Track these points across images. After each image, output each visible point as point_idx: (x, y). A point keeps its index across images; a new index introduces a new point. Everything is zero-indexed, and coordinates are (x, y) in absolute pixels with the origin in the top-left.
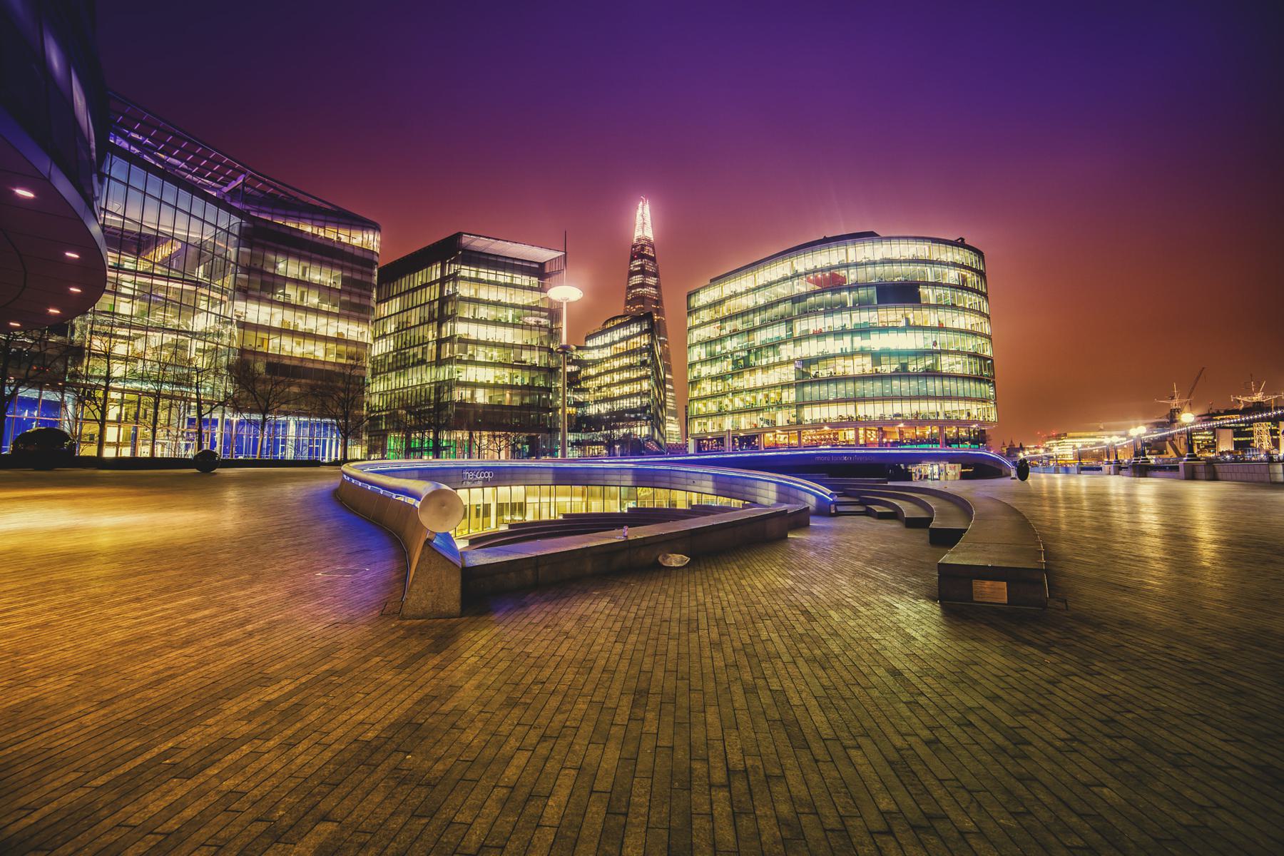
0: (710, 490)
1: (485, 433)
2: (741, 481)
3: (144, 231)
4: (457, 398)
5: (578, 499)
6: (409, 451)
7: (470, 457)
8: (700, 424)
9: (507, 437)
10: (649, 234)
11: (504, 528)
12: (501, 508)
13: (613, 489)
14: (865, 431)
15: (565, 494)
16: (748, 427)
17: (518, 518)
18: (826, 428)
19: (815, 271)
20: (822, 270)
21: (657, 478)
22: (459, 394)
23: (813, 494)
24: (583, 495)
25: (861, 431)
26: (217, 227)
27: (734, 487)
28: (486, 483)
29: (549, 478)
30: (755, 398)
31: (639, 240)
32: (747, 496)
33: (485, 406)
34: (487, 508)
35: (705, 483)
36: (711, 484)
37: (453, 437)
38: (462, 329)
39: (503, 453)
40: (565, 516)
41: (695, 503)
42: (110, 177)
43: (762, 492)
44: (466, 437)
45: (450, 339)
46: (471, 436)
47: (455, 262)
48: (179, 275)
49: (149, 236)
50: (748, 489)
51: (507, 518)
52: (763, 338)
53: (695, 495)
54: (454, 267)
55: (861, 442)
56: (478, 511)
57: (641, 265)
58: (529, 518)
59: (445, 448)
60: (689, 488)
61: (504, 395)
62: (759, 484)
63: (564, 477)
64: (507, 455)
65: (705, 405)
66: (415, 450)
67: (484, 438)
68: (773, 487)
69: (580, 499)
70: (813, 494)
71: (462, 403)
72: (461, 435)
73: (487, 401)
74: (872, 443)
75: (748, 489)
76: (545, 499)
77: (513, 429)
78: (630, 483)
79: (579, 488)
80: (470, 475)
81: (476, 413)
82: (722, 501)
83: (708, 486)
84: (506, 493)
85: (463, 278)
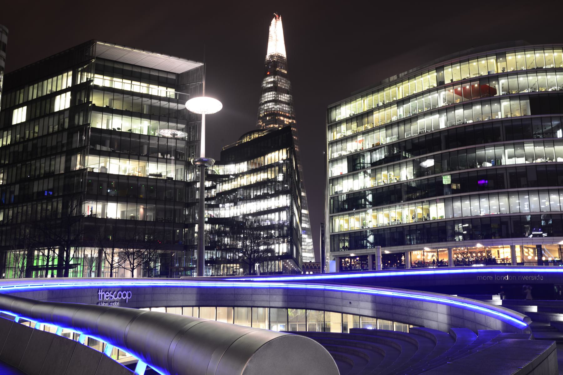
0: (369, 312)
1: (116, 250)
2: (339, 295)
4: (87, 213)
6: (29, 270)
7: (98, 274)
9: (140, 255)
10: (283, 52)
13: (261, 310)
14: (522, 248)
19: (463, 82)
20: (471, 80)
22: (77, 117)
25: (518, 248)
27: (396, 309)
30: (401, 214)
31: (272, 56)
32: (412, 320)
33: (116, 221)
35: (362, 304)
36: (369, 305)
37: (80, 255)
39: (135, 271)
43: (430, 315)
44: (96, 255)
46: (100, 253)
47: (88, 71)
50: (412, 311)
53: (350, 317)
54: (86, 76)
55: (519, 260)
57: (273, 82)
59: (71, 266)
60: (345, 309)
61: (137, 210)
62: (425, 305)
64: (139, 274)
65: (348, 222)
66: (37, 268)
67: (113, 255)
71: (92, 218)
72: (91, 252)
73: (119, 216)
74: (530, 262)
75: (412, 311)
77: (149, 245)
78: (280, 304)
81: (147, 187)
82: (381, 324)
83: (367, 308)
85: (96, 87)
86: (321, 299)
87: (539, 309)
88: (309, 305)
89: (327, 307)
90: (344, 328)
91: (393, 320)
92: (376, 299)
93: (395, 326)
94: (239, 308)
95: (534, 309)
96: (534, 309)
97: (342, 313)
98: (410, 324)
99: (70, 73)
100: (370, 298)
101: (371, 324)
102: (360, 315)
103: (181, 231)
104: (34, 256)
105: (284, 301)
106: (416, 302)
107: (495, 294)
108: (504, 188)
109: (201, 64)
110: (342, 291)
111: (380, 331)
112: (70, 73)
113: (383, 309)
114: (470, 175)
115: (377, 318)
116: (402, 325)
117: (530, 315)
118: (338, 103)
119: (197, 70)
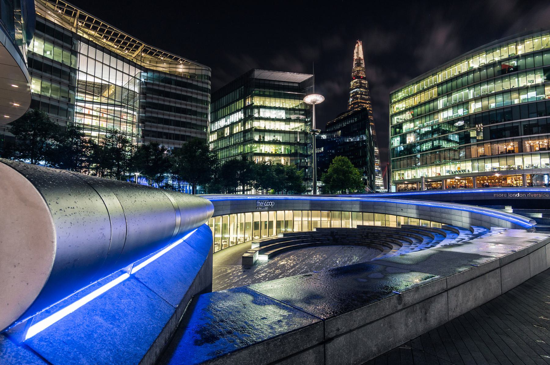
0: (415, 216)
2: (439, 210)
3: (104, 82)
5: (325, 219)
8: (399, 175)
11: (281, 236)
12: (279, 224)
15: (317, 216)
16: (434, 175)
17: (289, 230)
18: (497, 175)
21: (376, 207)
22: (258, 160)
23: (508, 220)
24: (328, 216)
26: (129, 75)
27: (433, 213)
28: (270, 209)
29: (357, 208)
32: (444, 220)
34: (271, 223)
35: (409, 210)
36: (415, 211)
38: (257, 124)
40: (317, 229)
41: (402, 223)
42: (80, 53)
43: (457, 218)
45: (250, 130)
48: (113, 102)
49: (106, 84)
50: (444, 215)
51: (283, 229)
52: (445, 116)
56: (266, 225)
58: (296, 230)
60: (398, 213)
62: (453, 212)
63: (315, 206)
64: (142, 116)
68: (467, 214)
69: (326, 219)
70: (508, 220)
75: (444, 215)
76: (305, 219)
79: (325, 213)
80: (261, 204)
83: (413, 212)
84: (281, 215)
86: (384, 207)
87: (543, 216)
88: (375, 211)
89: (387, 212)
90: (399, 224)
91: (431, 221)
92: (418, 207)
93: (432, 224)
94: (335, 212)
95: (540, 216)
96: (540, 216)
97: (397, 215)
98: (442, 223)
99: (243, 100)
100: (415, 207)
101: (414, 222)
102: (408, 217)
103: (372, 121)
104: (134, 172)
105: (360, 208)
106: (446, 210)
107: (507, 205)
108: (519, 136)
109: (311, 76)
110: (396, 203)
111: (422, 227)
112: (243, 100)
113: (423, 213)
114: (506, 126)
115: (420, 219)
116: (437, 224)
117: (536, 219)
118: (400, 88)
119: (309, 79)
